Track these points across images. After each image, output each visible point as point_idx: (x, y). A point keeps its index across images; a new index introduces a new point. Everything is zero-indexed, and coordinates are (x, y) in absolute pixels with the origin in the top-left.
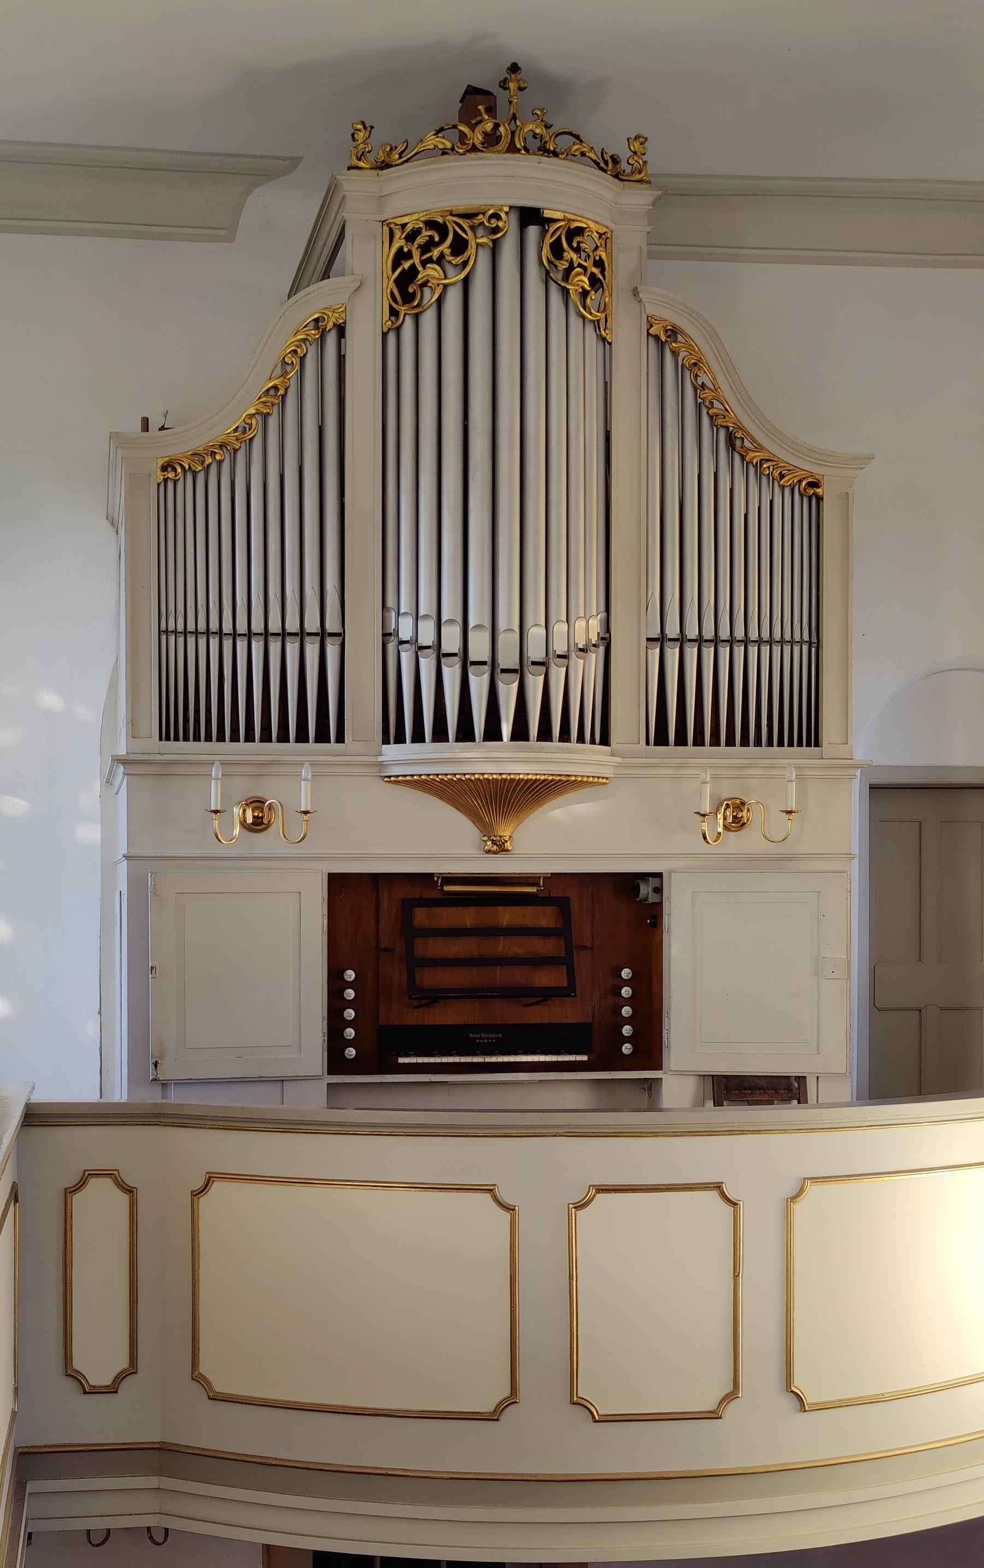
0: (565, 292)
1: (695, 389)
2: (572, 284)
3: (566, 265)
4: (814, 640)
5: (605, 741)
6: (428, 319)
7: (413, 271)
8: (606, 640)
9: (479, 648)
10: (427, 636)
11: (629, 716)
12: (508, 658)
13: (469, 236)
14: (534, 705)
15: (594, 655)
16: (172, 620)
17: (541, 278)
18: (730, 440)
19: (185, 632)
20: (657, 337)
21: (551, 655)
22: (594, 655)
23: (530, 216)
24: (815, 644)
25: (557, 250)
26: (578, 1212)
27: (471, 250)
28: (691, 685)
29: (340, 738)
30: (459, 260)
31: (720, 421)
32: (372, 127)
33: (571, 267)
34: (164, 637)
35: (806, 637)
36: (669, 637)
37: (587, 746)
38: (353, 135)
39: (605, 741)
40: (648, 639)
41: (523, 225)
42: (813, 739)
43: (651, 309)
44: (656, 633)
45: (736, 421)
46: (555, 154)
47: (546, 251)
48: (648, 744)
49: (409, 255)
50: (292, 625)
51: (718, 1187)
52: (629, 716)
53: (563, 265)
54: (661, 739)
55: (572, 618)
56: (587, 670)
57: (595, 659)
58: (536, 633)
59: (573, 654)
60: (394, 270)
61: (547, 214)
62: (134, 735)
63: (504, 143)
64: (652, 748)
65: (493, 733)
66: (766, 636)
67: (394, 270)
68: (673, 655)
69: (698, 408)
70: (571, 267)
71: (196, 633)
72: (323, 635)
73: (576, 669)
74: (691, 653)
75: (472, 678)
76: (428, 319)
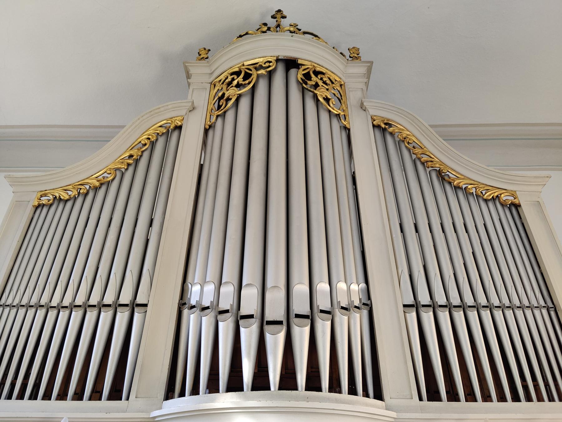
1: (409, 150)
2: (318, 91)
4: (551, 305)
5: (379, 396)
6: (230, 115)
7: (224, 94)
8: (368, 305)
11: (398, 370)
12: (275, 311)
14: (301, 351)
15: (358, 315)
17: (299, 90)
18: (439, 173)
20: (379, 126)
21: (315, 310)
22: (358, 315)
23: (291, 64)
27: (254, 77)
28: (458, 375)
29: (128, 399)
30: (247, 82)
32: (209, 50)
36: (422, 303)
37: (360, 398)
38: (199, 53)
39: (379, 396)
40: (405, 306)
41: (287, 70)
43: (372, 112)
44: (410, 300)
45: (441, 163)
48: (421, 399)
52: (398, 370)
54: (434, 395)
56: (350, 327)
57: (359, 319)
58: (300, 288)
59: (337, 310)
61: (300, 62)
64: (425, 403)
65: (261, 382)
68: (428, 317)
69: (414, 162)
72: (134, 306)
73: (342, 325)
75: (242, 330)
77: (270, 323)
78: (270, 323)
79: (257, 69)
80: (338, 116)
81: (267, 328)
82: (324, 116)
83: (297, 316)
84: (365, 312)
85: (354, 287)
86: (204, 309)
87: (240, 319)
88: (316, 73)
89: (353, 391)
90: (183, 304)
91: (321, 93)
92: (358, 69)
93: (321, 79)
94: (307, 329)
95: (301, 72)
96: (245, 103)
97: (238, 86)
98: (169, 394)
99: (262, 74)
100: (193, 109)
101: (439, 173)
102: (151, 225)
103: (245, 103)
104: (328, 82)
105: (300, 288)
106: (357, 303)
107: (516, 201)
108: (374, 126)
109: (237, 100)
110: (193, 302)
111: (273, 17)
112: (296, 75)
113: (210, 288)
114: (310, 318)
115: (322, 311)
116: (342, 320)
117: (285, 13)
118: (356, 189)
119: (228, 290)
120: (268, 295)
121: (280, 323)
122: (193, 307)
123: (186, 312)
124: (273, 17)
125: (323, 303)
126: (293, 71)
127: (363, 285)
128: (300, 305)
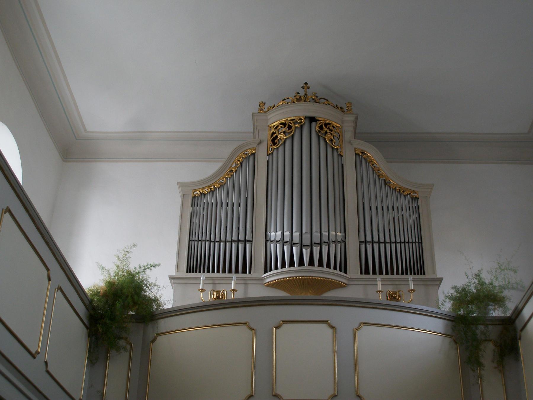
0: (325, 140)
3: (324, 132)
4: (420, 241)
5: (346, 272)
6: (281, 150)
7: (277, 136)
8: (344, 242)
9: (296, 239)
10: (279, 238)
13: (292, 125)
16: (193, 237)
18: (385, 181)
19: (198, 241)
23: (312, 120)
24: (420, 243)
25: (321, 128)
26: (278, 330)
27: (293, 128)
29: (250, 272)
30: (290, 131)
31: (380, 177)
33: (326, 132)
34: (191, 242)
35: (417, 241)
39: (346, 272)
42: (423, 272)
43: (355, 146)
46: (319, 103)
47: (317, 128)
49: (275, 133)
50: (235, 238)
51: (326, 322)
53: (323, 132)
55: (330, 231)
60: (271, 137)
61: (317, 119)
62: (178, 269)
63: (303, 100)
66: (402, 240)
67: (271, 137)
70: (326, 132)
71: (202, 241)
72: (245, 241)
74: (376, 246)
76: (281, 150)
77: (304, 246)
78: (304, 246)
79: (295, 123)
80: (337, 149)
81: (303, 247)
82: (329, 150)
83: (315, 243)
84: (343, 244)
85: (339, 234)
86: (277, 241)
87: (292, 244)
88: (326, 125)
89: (335, 268)
90: (266, 241)
91: (329, 136)
92: (349, 118)
93: (329, 128)
94: (319, 248)
95: (318, 125)
96: (288, 143)
97: (284, 132)
98: (266, 272)
99: (297, 127)
100: (260, 143)
101: (385, 181)
102: (233, 206)
103: (288, 143)
104: (332, 128)
105: (316, 235)
106: (339, 240)
107: (417, 196)
108: (356, 154)
109: (284, 143)
110: (272, 239)
111: (303, 87)
112: (315, 127)
113: (279, 233)
114: (320, 245)
115: (324, 242)
116: (333, 246)
117: (309, 85)
118: (40, 392)
119: (287, 233)
120: (303, 236)
121: (308, 246)
122: (271, 241)
123: (268, 243)
124: (303, 87)
125: (325, 239)
126: (314, 124)
127: (343, 234)
128: (316, 239)
